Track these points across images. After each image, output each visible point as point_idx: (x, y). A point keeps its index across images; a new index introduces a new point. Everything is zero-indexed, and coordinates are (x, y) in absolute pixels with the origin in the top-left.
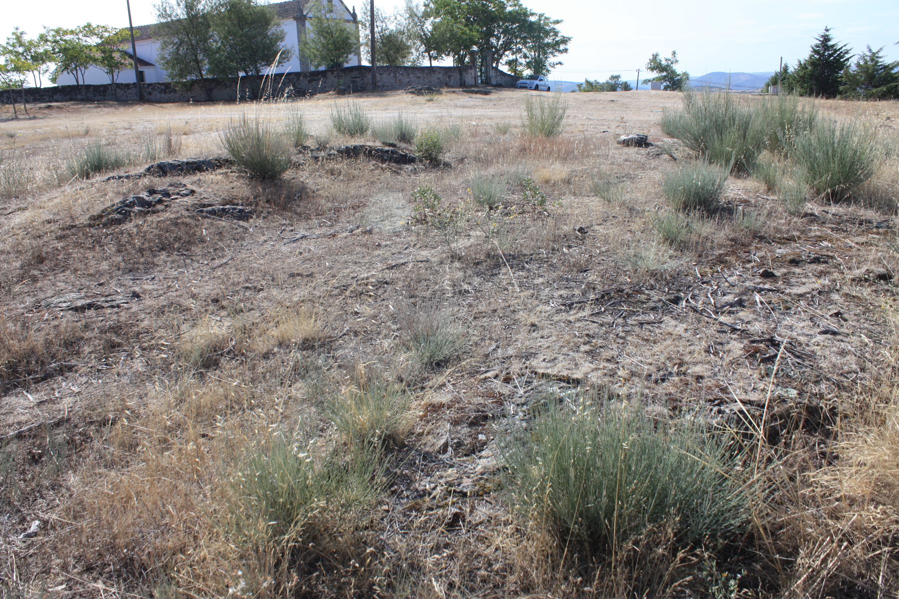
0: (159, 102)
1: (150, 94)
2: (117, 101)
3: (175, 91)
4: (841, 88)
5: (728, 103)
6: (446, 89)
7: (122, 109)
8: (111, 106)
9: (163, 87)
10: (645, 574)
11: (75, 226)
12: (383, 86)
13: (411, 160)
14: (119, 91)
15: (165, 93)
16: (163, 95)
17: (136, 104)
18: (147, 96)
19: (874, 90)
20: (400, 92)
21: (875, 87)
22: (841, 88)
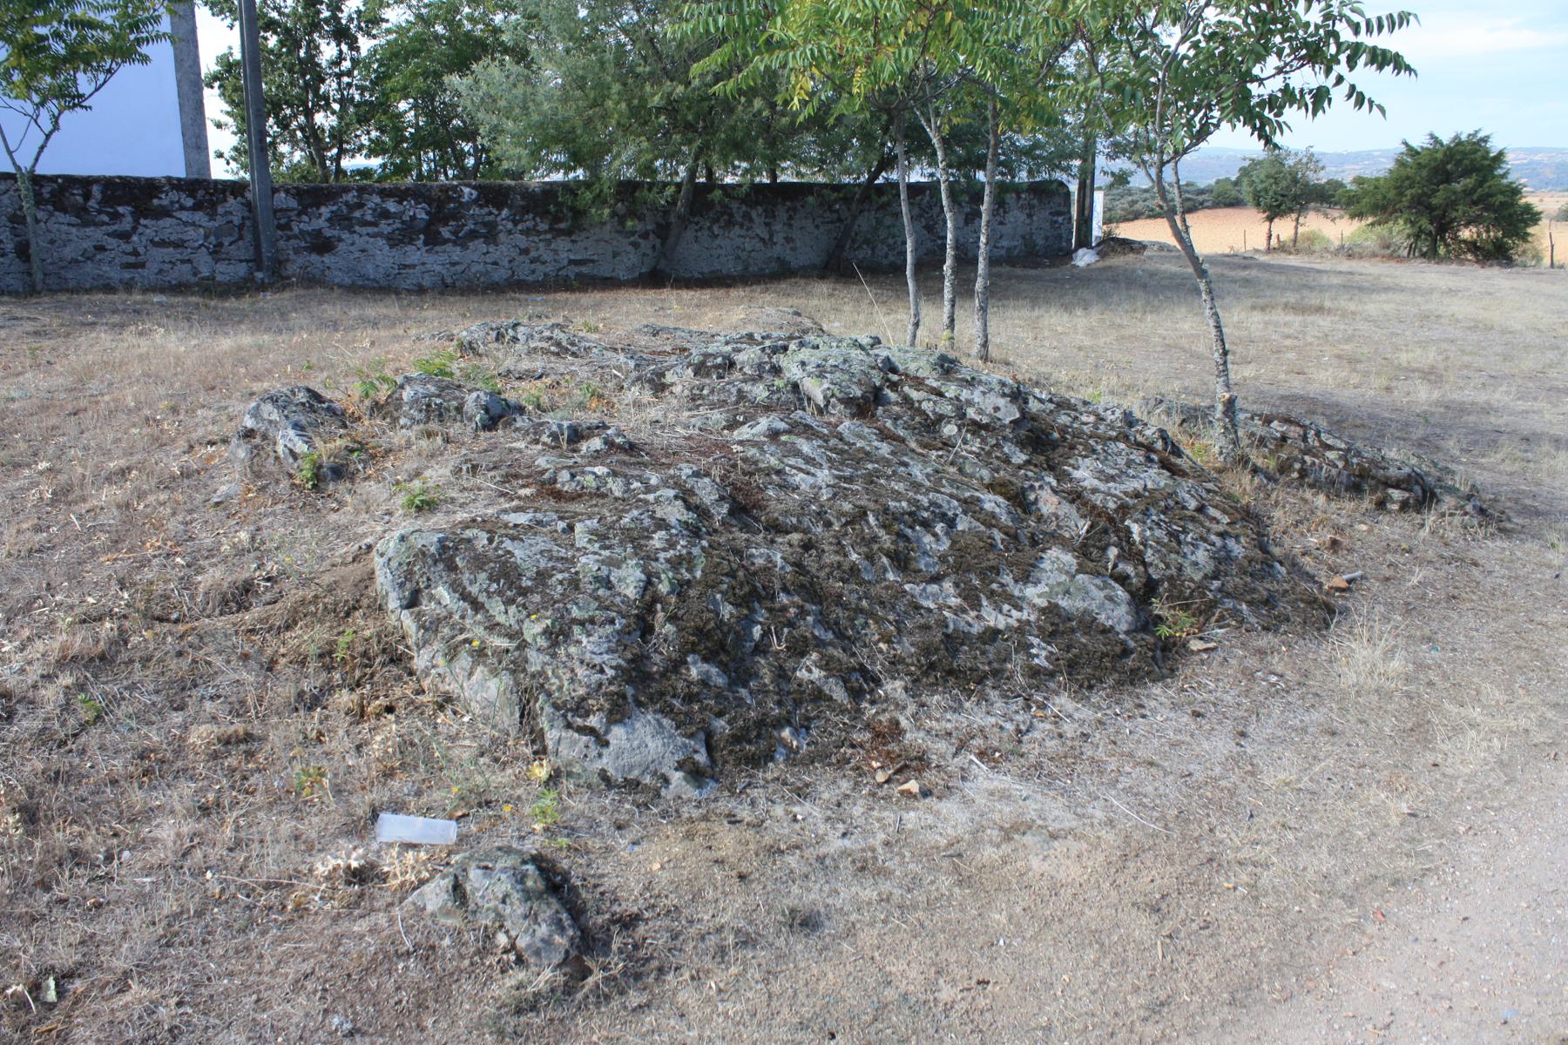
15: (433, 240)
16: (415, 254)
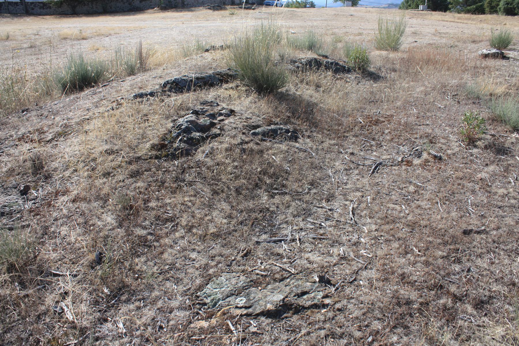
0: (40, 15)
1: (33, 9)
2: (9, 13)
3: (50, 8)
4: (450, 6)
5: (81, 57)
6: (230, 6)
7: (16, 19)
8: (6, 17)
9: (42, 5)
10: (122, 1)
11: (139, 158)
12: (188, 4)
13: (349, 71)
14: (10, 7)
15: (43, 9)
16: (42, 10)
17: (24, 16)
18: (31, 11)
19: (469, 8)
20: (201, 8)
21: (470, 6)
22: (450, 6)
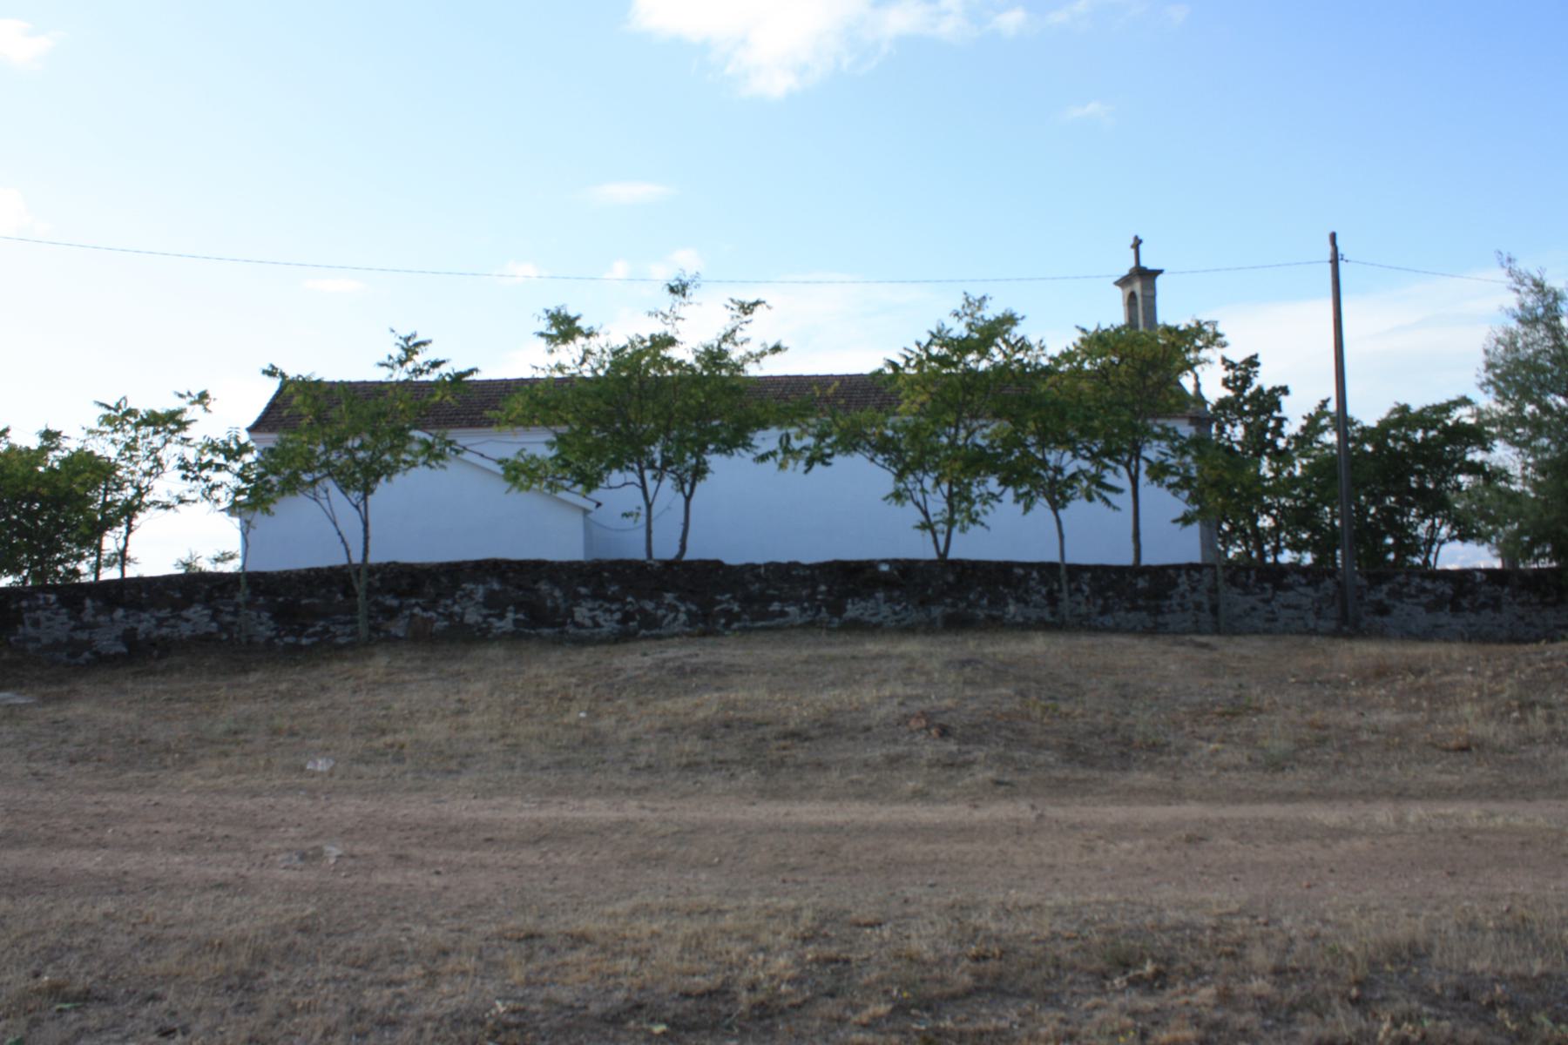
16: (1444, 618)
